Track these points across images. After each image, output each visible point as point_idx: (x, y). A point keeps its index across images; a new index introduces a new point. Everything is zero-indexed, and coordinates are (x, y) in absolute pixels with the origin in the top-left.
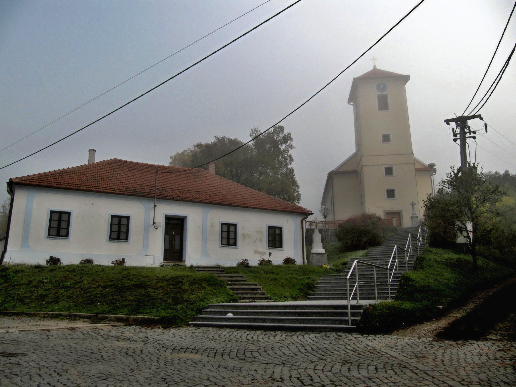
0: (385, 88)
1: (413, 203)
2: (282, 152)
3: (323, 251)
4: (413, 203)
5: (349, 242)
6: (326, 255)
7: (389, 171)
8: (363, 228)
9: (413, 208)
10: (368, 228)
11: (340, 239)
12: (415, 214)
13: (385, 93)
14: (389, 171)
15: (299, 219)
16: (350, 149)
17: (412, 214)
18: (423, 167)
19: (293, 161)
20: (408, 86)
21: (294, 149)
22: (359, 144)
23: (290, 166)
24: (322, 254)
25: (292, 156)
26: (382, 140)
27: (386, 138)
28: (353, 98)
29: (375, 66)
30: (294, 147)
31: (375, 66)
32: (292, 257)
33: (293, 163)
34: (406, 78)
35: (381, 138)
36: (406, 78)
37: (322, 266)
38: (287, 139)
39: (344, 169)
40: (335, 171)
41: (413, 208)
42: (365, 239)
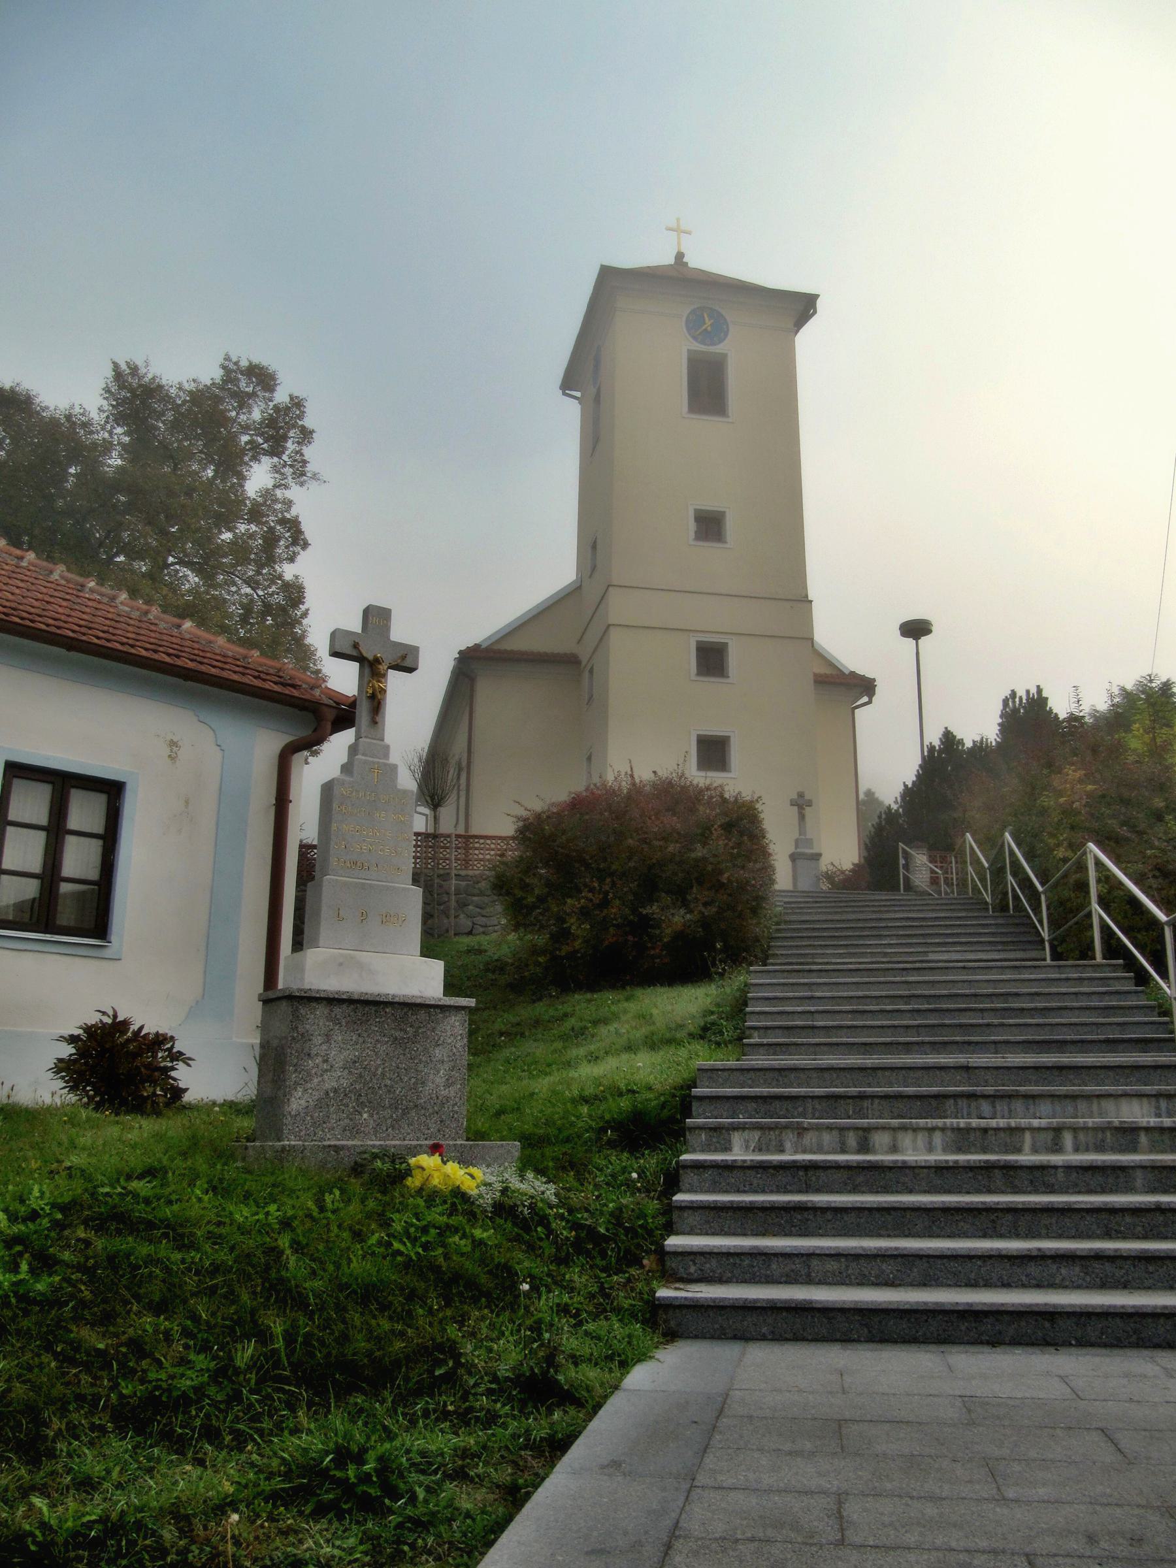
0: (719, 331)
1: (801, 795)
2: (255, 504)
3: (424, 979)
4: (801, 795)
5: (580, 929)
6: (455, 1029)
7: (712, 659)
8: (672, 848)
9: (802, 817)
10: (699, 852)
11: (521, 913)
12: (809, 842)
13: (718, 349)
14: (712, 659)
15: (261, 743)
16: (552, 567)
17: (797, 843)
18: (828, 671)
19: (306, 545)
20: (807, 340)
21: (313, 485)
22: (592, 548)
23: (289, 571)
24: (353, 750)
25: (304, 527)
26: (692, 534)
27: (710, 526)
28: (585, 372)
29: (680, 256)
30: (315, 477)
31: (680, 256)
32: (148, 1019)
33: (304, 557)
34: (801, 307)
35: (692, 526)
36: (801, 307)
37: (389, 1177)
38: (283, 430)
39: (519, 645)
40: (487, 650)
41: (802, 817)
42: (676, 919)
